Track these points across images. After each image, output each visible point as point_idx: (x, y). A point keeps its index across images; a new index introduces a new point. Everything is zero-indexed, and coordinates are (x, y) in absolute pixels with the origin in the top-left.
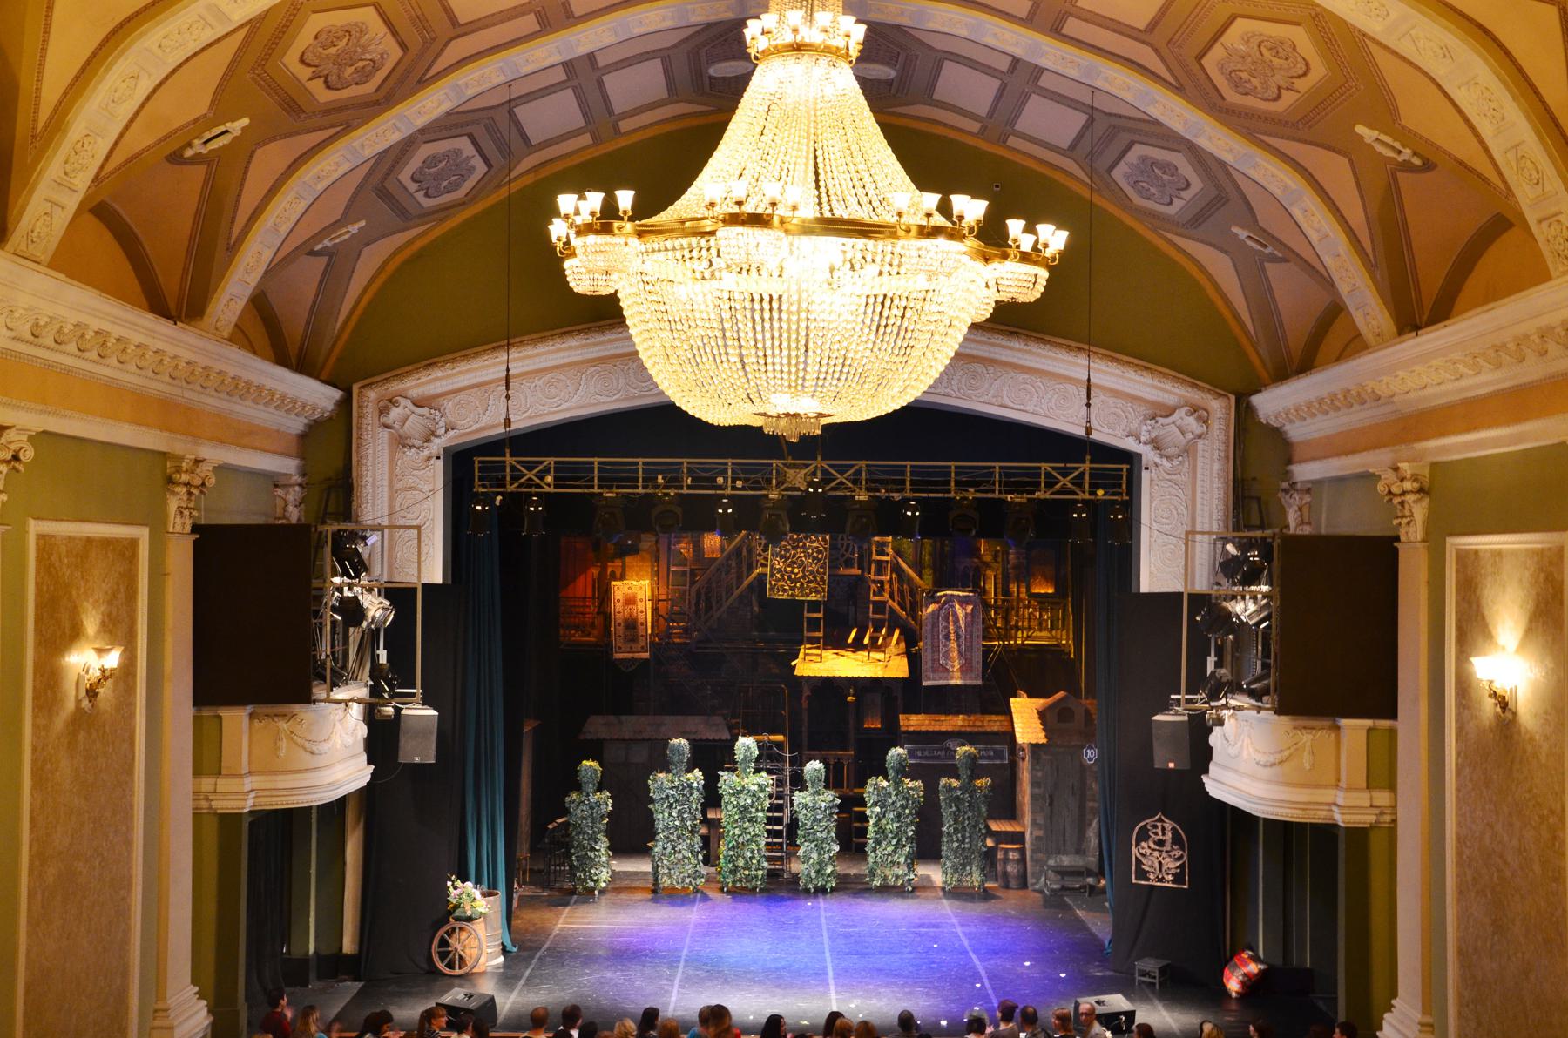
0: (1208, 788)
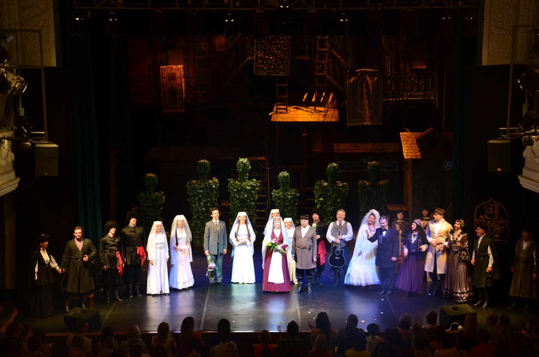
0: (521, 183)
